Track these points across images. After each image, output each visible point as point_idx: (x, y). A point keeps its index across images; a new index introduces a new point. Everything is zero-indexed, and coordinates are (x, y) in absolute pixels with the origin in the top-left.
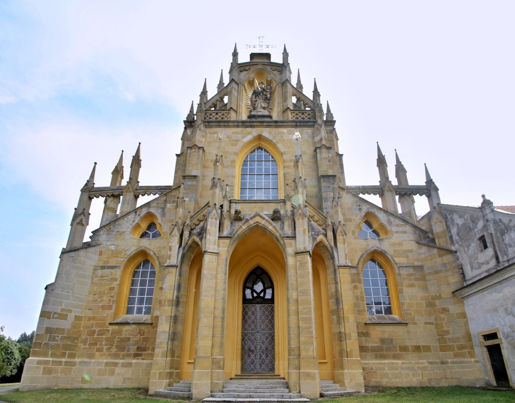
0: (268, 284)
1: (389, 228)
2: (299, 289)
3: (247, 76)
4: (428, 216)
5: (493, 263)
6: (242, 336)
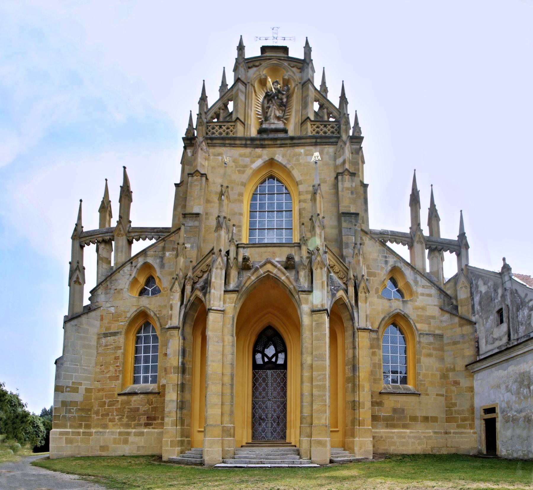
0: (280, 348)
1: (414, 288)
2: (314, 353)
3: (258, 73)
4: (455, 279)
5: (505, 339)
6: (253, 404)
